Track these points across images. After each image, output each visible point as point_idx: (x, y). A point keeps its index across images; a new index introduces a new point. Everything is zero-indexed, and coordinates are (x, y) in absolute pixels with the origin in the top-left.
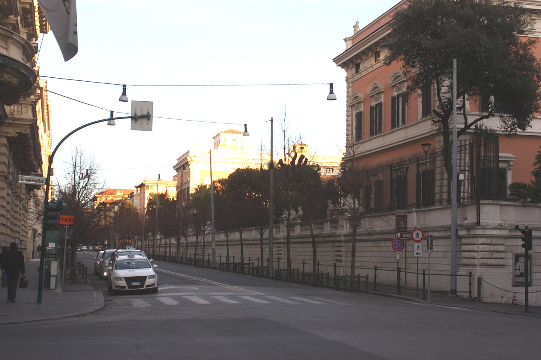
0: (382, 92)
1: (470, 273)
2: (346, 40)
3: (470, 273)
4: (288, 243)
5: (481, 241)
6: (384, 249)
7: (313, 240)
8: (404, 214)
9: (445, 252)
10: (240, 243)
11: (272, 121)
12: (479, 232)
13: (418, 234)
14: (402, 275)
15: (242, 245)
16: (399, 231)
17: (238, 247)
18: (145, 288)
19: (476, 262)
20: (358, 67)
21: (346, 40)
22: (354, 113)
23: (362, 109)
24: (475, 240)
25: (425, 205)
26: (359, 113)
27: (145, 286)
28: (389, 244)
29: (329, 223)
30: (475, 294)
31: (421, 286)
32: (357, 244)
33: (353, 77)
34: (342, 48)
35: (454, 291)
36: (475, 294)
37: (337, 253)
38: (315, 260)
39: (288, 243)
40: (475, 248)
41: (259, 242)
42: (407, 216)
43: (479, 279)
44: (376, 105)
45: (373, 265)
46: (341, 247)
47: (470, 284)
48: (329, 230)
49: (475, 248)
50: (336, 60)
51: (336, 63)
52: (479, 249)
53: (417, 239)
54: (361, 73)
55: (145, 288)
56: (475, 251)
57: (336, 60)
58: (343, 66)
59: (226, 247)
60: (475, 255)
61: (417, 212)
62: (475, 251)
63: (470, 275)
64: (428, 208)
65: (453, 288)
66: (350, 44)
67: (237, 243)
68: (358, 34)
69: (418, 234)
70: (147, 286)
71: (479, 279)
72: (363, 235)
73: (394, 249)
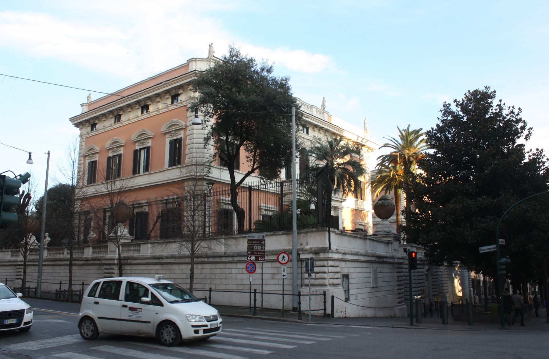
0: (122, 146)
1: (325, 292)
2: (82, 105)
3: (325, 292)
4: (25, 265)
5: (331, 263)
6: (178, 271)
7: (120, 262)
8: (262, 238)
9: (273, 274)
10: (23, 263)
11: (49, 154)
12: (330, 255)
13: (284, 257)
14: (258, 296)
15: (71, 265)
16: (252, 254)
17: (184, 267)
18: (22, 326)
19: (326, 282)
20: (93, 126)
21: (82, 105)
22: (87, 162)
23: (97, 159)
24: (325, 263)
25: (166, 238)
26: (93, 162)
27: (23, 323)
28: (244, 265)
29: (46, 250)
30: (329, 311)
31: (253, 305)
32: (195, 266)
33: (88, 134)
34: (78, 111)
35: (297, 310)
36: (329, 311)
37: (18, 273)
38: (70, 281)
39: (25, 265)
40: (326, 269)
41: (23, 263)
42: (264, 241)
43: (333, 297)
44: (113, 156)
45: (207, 287)
46: (113, 269)
47: (325, 302)
48: (91, 254)
49: (326, 269)
50: (72, 120)
51: (72, 122)
52: (329, 272)
53: (283, 262)
54: (97, 131)
55: (22, 326)
56: (325, 273)
57: (72, 120)
58: (77, 125)
59: (68, 267)
60: (326, 276)
61: (225, 239)
62: (325, 273)
63: (324, 294)
64: (244, 236)
65: (296, 305)
66: (86, 109)
67: (76, 262)
68: (89, 104)
69: (284, 257)
70: (26, 323)
71: (333, 297)
72: (201, 257)
73: (248, 271)
